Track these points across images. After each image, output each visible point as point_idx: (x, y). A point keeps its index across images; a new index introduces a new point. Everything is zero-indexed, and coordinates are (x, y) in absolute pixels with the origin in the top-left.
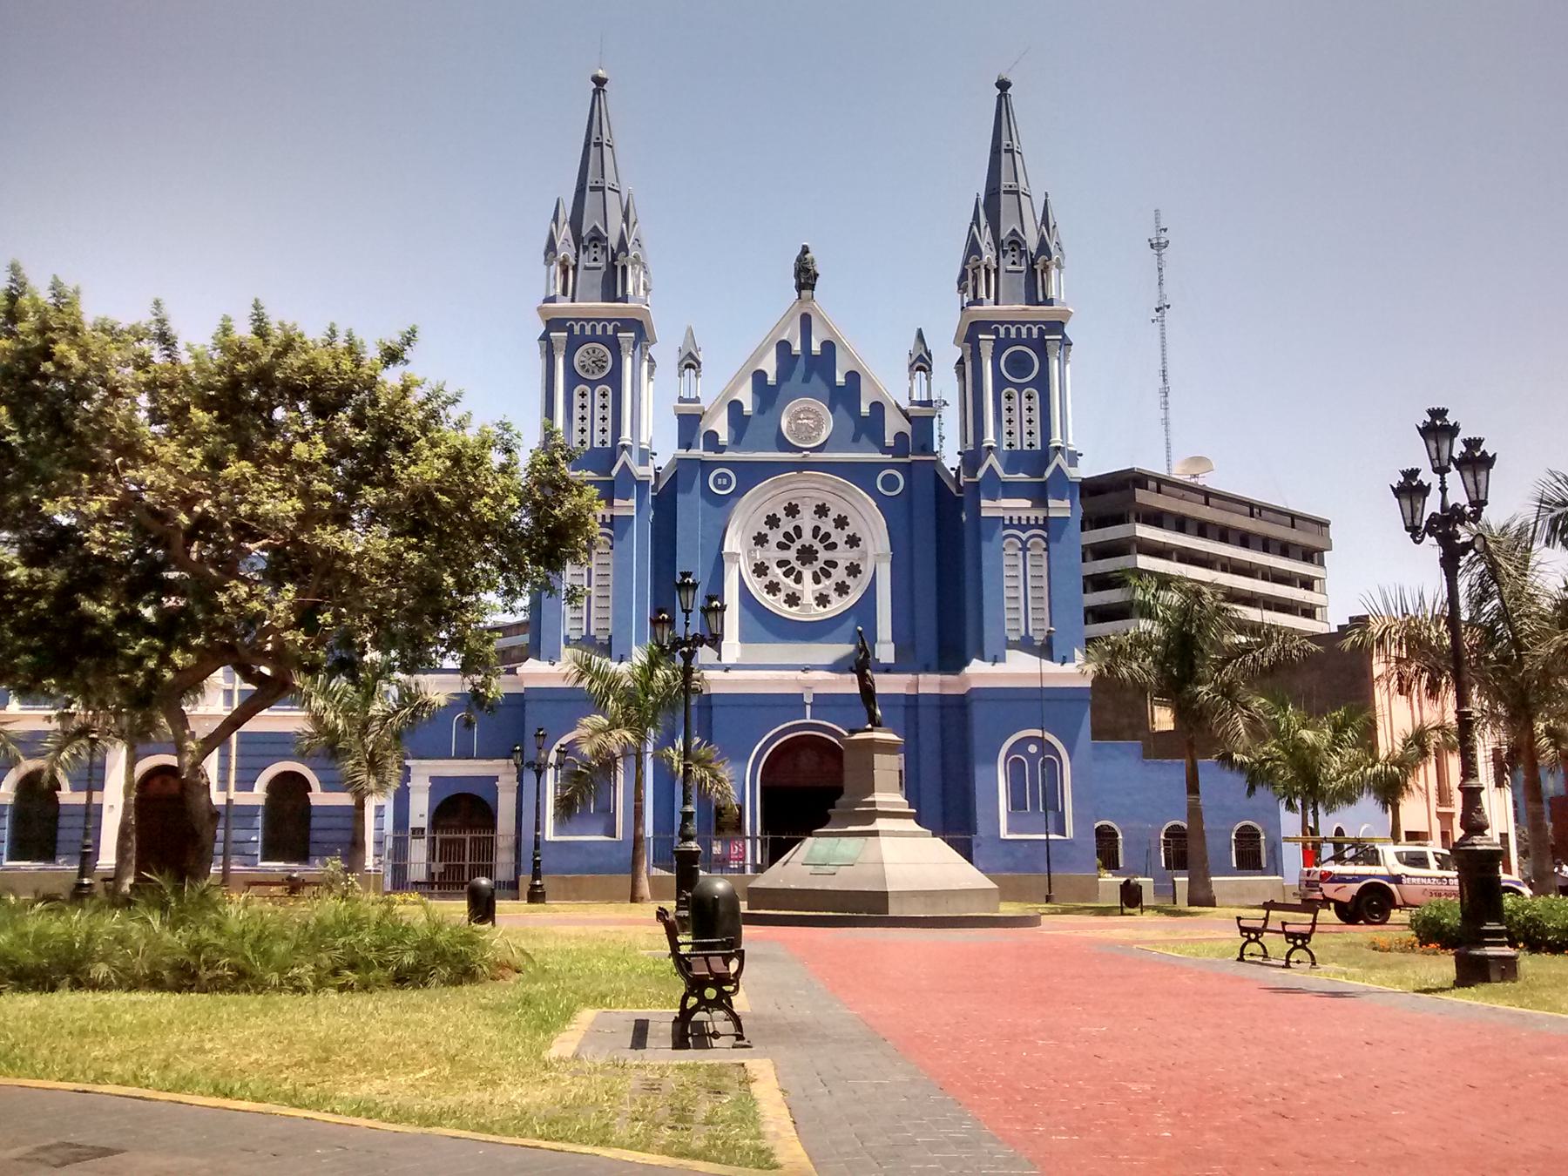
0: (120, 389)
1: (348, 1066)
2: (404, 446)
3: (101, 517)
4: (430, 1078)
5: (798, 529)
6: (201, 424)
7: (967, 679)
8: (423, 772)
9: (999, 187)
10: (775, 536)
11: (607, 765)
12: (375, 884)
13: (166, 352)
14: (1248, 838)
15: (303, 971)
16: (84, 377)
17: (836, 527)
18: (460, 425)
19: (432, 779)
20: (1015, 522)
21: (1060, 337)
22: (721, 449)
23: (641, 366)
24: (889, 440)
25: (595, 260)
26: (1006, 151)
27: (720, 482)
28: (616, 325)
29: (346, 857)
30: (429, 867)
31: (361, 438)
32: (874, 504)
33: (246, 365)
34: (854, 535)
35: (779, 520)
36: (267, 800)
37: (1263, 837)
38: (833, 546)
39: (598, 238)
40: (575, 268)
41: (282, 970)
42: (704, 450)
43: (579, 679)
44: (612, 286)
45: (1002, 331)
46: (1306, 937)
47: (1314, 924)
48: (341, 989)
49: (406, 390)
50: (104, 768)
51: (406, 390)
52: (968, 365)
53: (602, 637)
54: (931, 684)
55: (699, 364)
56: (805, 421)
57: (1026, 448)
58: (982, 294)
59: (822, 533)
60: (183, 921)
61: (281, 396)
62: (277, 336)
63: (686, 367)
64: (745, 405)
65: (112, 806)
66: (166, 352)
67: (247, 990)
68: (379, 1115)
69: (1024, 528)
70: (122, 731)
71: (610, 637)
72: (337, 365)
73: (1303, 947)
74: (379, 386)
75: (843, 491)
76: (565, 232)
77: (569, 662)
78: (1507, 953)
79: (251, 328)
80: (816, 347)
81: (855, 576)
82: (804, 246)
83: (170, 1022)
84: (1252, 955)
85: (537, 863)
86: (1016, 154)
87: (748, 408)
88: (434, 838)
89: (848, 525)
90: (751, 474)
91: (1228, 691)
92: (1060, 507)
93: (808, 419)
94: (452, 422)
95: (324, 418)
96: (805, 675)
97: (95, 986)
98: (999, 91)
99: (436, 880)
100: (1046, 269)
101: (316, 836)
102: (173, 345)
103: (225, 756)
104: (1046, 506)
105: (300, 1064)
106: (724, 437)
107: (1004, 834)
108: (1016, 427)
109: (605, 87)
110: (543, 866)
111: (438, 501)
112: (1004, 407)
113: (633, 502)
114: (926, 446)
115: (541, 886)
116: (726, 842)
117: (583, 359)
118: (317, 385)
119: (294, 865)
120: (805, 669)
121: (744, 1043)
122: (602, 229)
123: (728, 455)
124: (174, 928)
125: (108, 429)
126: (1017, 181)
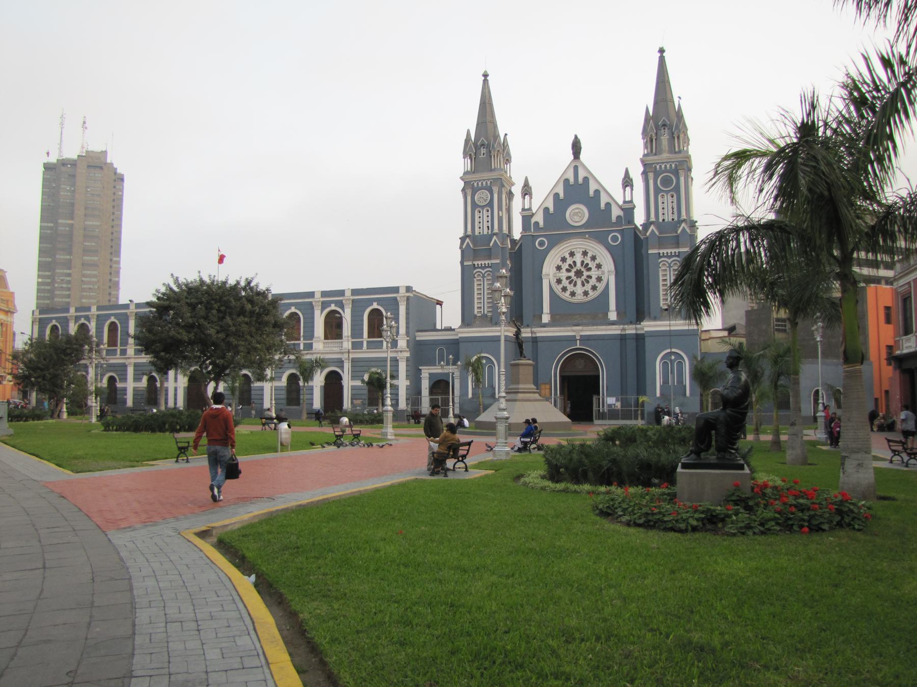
10: (565, 266)
20: (665, 255)
36: (148, 385)
54: (631, 330)
80: (580, 180)
81: (600, 282)
90: (555, 241)
112: (490, 217)
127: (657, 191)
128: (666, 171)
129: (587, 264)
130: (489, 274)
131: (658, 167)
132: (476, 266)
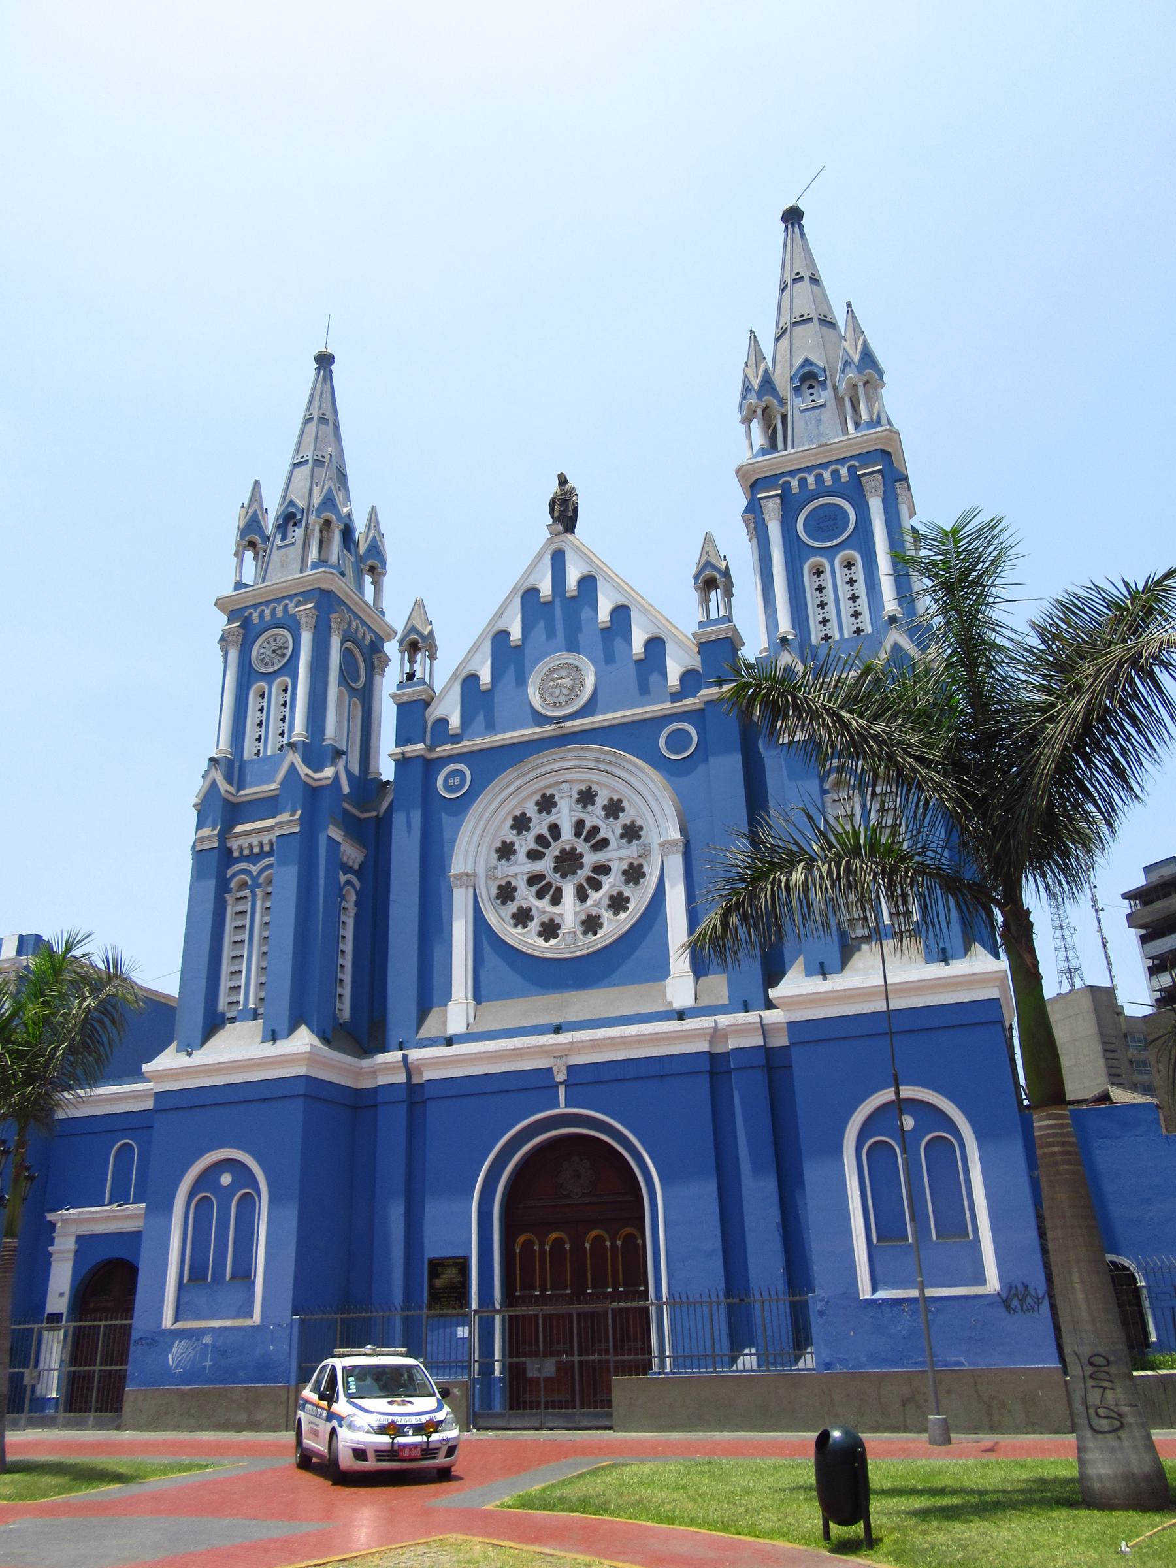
12: (1062, 1124)
75: (610, 763)
107: (865, 1292)
117: (262, 650)
120: (557, 1030)
123: (466, 745)
127: (795, 553)
129: (595, 830)
131: (794, 483)
132: (236, 854)
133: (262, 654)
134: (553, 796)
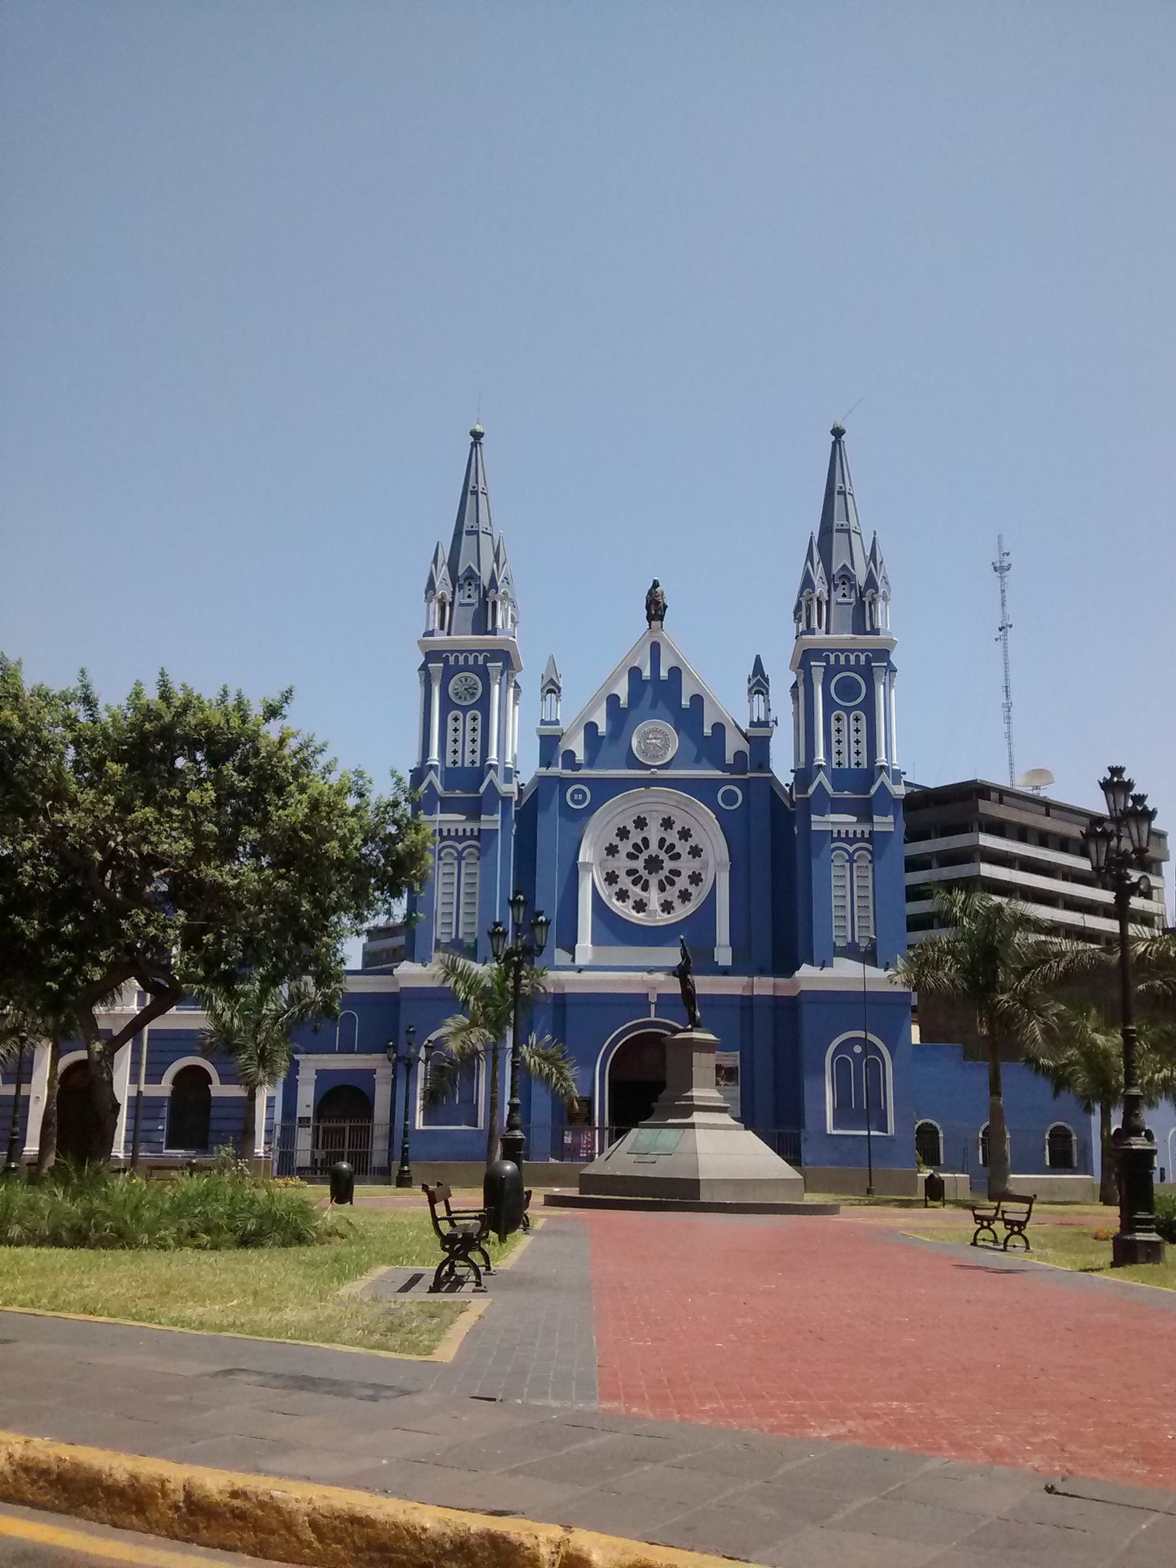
0: (51, 746)
1: (182, 1297)
2: (280, 790)
3: (32, 854)
4: (238, 1306)
5: (645, 841)
6: (115, 775)
7: (796, 984)
8: (311, 1065)
9: (832, 526)
10: (625, 847)
11: (469, 1060)
13: (90, 712)
14: (1060, 1139)
15: (167, 1232)
16: (23, 737)
17: (680, 839)
18: (328, 770)
19: (317, 1072)
20: (843, 836)
21: (885, 664)
22: (578, 767)
23: (507, 691)
24: (729, 758)
25: (469, 596)
26: (839, 493)
27: (576, 798)
28: (485, 656)
29: (236, 1145)
30: (313, 1154)
31: (244, 784)
32: (714, 816)
33: (153, 725)
34: (696, 846)
35: (629, 832)
37: (1074, 1138)
38: (677, 857)
39: (471, 577)
40: (452, 604)
41: (151, 1233)
42: (562, 769)
43: (445, 980)
44: (482, 622)
45: (832, 658)
46: (1022, 1225)
47: (1029, 1213)
48: (198, 1247)
49: (282, 742)
50: (32, 1063)
51: (282, 742)
52: (801, 689)
53: (469, 940)
54: (764, 986)
55: (559, 689)
56: (654, 741)
57: (853, 766)
58: (815, 624)
59: (667, 844)
60: (81, 1193)
61: (181, 748)
62: (179, 696)
63: (548, 693)
64: (599, 727)
65: (38, 1098)
66: (90, 712)
67: (123, 1248)
68: (189, 1325)
69: (851, 841)
70: (47, 1030)
71: (476, 941)
72: (228, 721)
73: (1019, 1233)
74: (261, 739)
75: (686, 805)
76: (443, 572)
77: (437, 964)
78: (1153, 1239)
79: (157, 692)
80: (664, 674)
81: (697, 885)
82: (655, 581)
83: (62, 1267)
84: (984, 1240)
85: (405, 1150)
86: (848, 496)
87: (602, 729)
88: (319, 1127)
89: (691, 836)
90: (604, 790)
91: (1025, 999)
92: (884, 823)
93: (655, 738)
94: (320, 767)
95: (215, 767)
96: (650, 976)
97: (10, 1242)
98: (833, 438)
99: (319, 1165)
100: (873, 602)
101: (214, 1125)
102: (95, 706)
103: (136, 1051)
104: (870, 820)
105: (147, 1296)
106: (580, 756)
108: (844, 747)
109: (482, 440)
110: (411, 1153)
111: (302, 838)
112: (833, 729)
113: (498, 817)
114: (763, 763)
115: (408, 1171)
116: (576, 1134)
117: (457, 687)
118: (211, 739)
119: (192, 1153)
121: (482, 1288)
122: (476, 570)
123: (584, 773)
124: (73, 1200)
125: (41, 780)
126: (848, 520)
128: (848, 667)
129: (672, 846)
130: (471, 854)
133: (456, 689)
134: (645, 819)
